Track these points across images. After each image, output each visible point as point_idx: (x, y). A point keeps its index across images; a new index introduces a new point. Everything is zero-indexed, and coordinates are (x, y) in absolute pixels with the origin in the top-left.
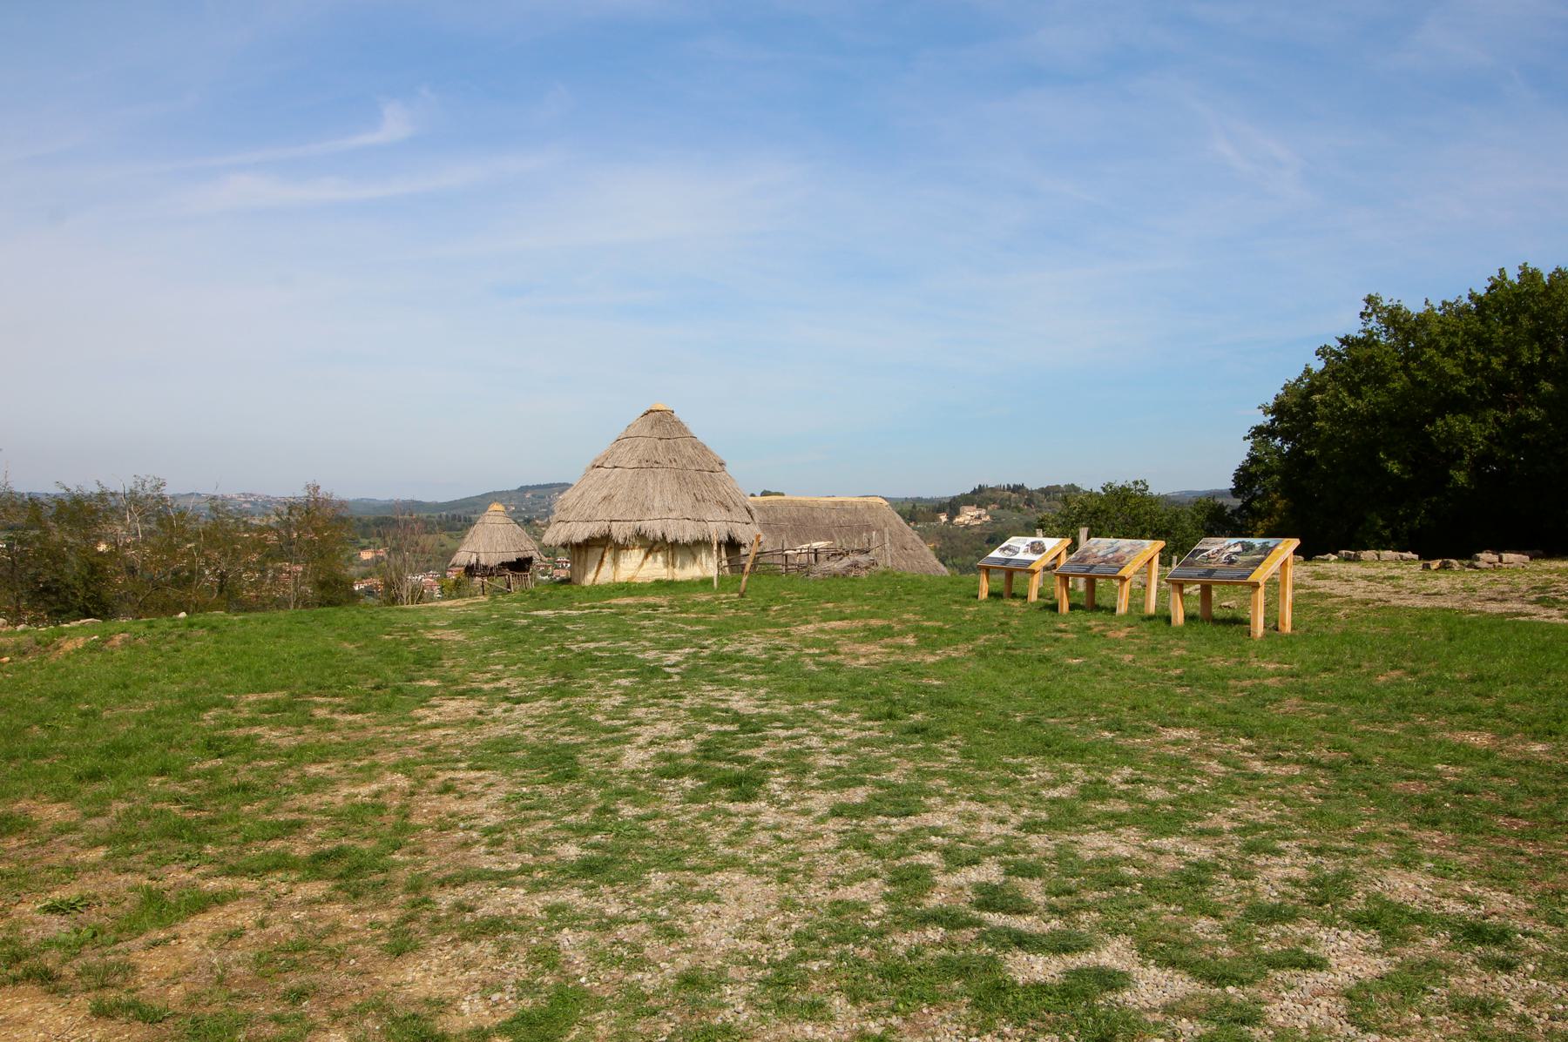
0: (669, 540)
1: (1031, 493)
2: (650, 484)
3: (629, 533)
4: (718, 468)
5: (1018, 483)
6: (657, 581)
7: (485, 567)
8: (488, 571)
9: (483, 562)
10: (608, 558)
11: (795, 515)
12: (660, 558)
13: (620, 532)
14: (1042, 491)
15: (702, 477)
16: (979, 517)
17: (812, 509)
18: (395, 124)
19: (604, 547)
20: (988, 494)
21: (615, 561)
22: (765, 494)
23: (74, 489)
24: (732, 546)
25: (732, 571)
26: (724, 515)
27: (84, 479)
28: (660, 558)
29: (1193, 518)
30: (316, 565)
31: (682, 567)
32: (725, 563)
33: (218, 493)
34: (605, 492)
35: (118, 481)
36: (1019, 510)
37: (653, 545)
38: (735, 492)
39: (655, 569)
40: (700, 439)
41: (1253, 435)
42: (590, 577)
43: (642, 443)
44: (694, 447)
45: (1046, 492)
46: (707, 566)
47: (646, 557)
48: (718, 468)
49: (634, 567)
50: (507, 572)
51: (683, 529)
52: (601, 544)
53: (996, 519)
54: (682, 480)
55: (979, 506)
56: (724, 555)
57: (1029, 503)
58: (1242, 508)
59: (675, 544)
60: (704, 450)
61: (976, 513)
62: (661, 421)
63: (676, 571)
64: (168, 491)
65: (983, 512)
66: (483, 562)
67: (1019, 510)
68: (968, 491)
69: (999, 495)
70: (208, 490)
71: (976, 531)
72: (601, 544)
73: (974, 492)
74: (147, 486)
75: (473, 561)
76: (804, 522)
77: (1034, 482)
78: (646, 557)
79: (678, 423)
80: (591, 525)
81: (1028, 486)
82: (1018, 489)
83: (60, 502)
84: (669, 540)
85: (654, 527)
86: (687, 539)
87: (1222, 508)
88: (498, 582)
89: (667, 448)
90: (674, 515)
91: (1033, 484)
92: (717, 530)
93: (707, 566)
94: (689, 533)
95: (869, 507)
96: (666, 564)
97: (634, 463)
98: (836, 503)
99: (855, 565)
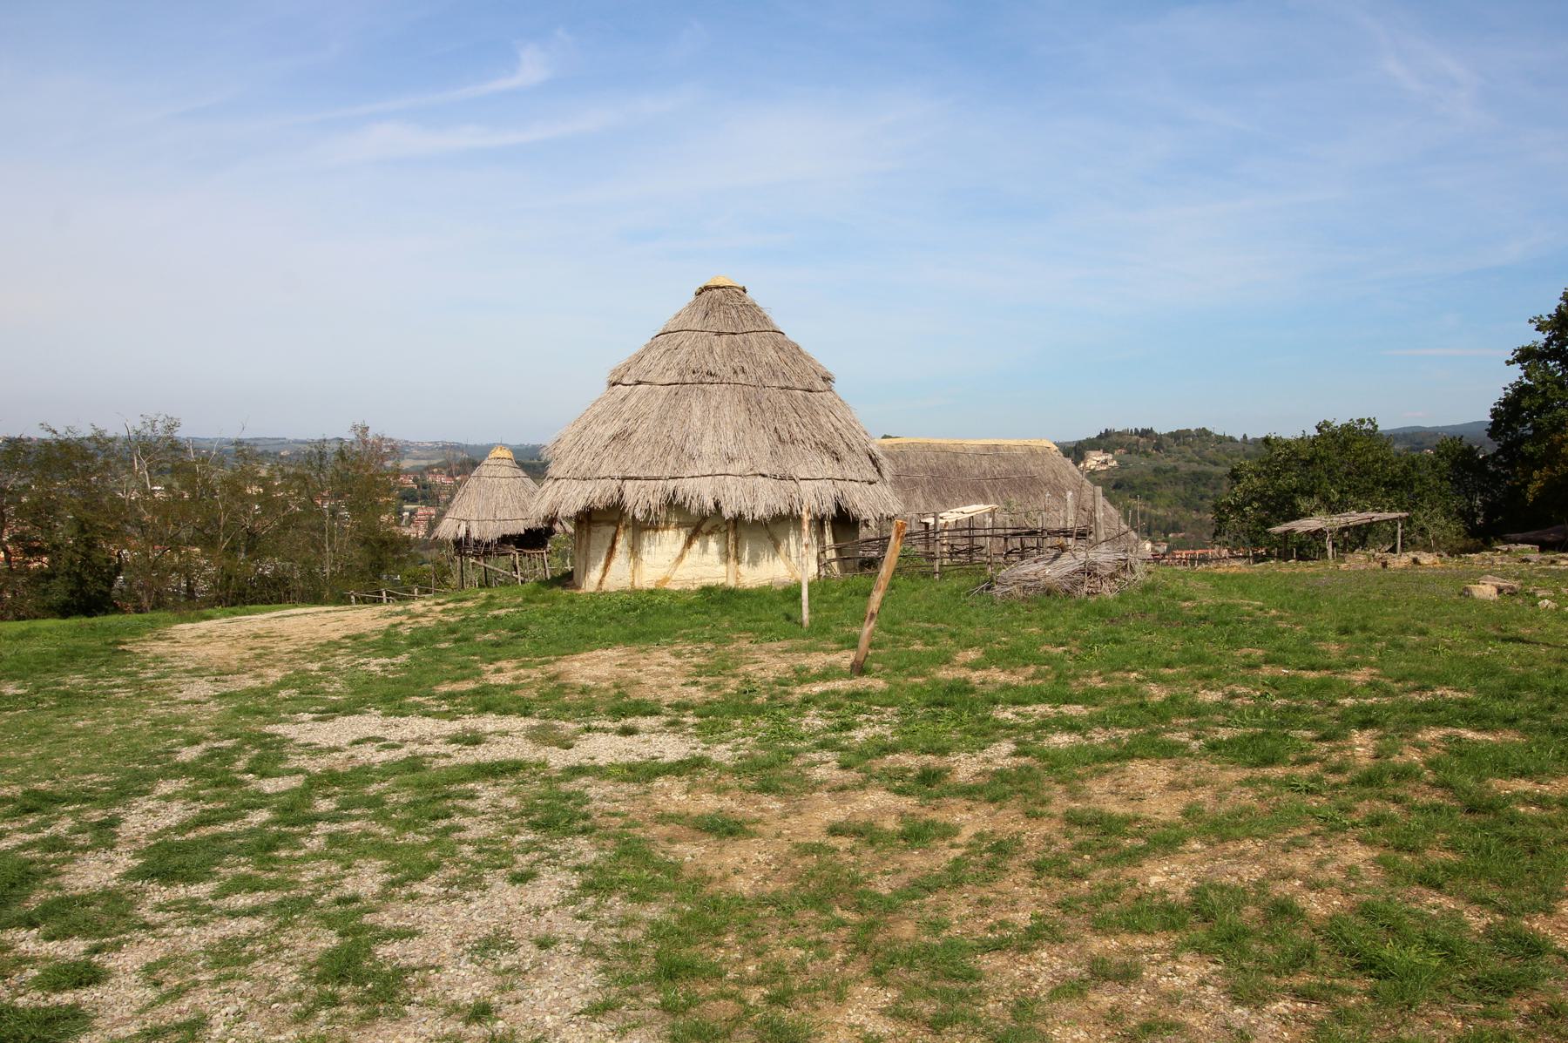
0: (727, 513)
1: (1160, 437)
2: (697, 411)
3: (654, 502)
4: (819, 384)
5: (1147, 427)
6: (707, 591)
7: (478, 542)
8: (484, 549)
9: (475, 535)
10: (622, 544)
11: (933, 463)
12: (713, 545)
13: (638, 498)
14: (1171, 435)
15: (791, 399)
16: (1105, 462)
17: (956, 455)
18: (532, 68)
19: (616, 524)
20: (1114, 438)
21: (635, 551)
22: (885, 437)
23: (61, 431)
24: (843, 522)
25: (844, 569)
26: (830, 468)
27: (75, 416)
28: (713, 545)
29: (1434, 466)
30: (323, 521)
31: (754, 560)
32: (831, 554)
33: (243, 436)
34: (615, 427)
35: (117, 425)
36: (1148, 455)
37: (701, 523)
38: (850, 426)
39: (698, 566)
40: (791, 336)
41: (1519, 360)
42: (594, 575)
43: (687, 341)
44: (779, 348)
45: (1177, 436)
46: (796, 564)
47: (689, 543)
48: (819, 384)
49: (668, 563)
50: (512, 549)
51: (754, 493)
52: (603, 521)
53: (1123, 465)
54: (752, 404)
55: (1106, 451)
56: (829, 539)
57: (1158, 447)
58: (1499, 452)
59: (738, 520)
60: (795, 353)
61: (1103, 458)
62: (722, 303)
63: (743, 568)
64: (181, 434)
65: (1110, 457)
66: (475, 535)
67: (1148, 455)
68: (1094, 435)
69: (1126, 439)
70: (234, 434)
71: (1103, 476)
72: (603, 521)
73: (1100, 437)
74: (159, 426)
75: (462, 533)
76: (942, 474)
77: (1163, 426)
78: (689, 543)
79: (752, 307)
80: (589, 486)
81: (1157, 431)
82: (1146, 433)
83: (46, 444)
84: (727, 513)
85: (701, 491)
86: (761, 512)
87: (1470, 452)
88: (498, 565)
89: (731, 350)
90: (737, 468)
91: (1162, 428)
92: (815, 496)
93: (796, 564)
94: (763, 500)
95: (1032, 453)
96: (725, 556)
97: (672, 376)
98: (987, 447)
99: (1089, 571)
